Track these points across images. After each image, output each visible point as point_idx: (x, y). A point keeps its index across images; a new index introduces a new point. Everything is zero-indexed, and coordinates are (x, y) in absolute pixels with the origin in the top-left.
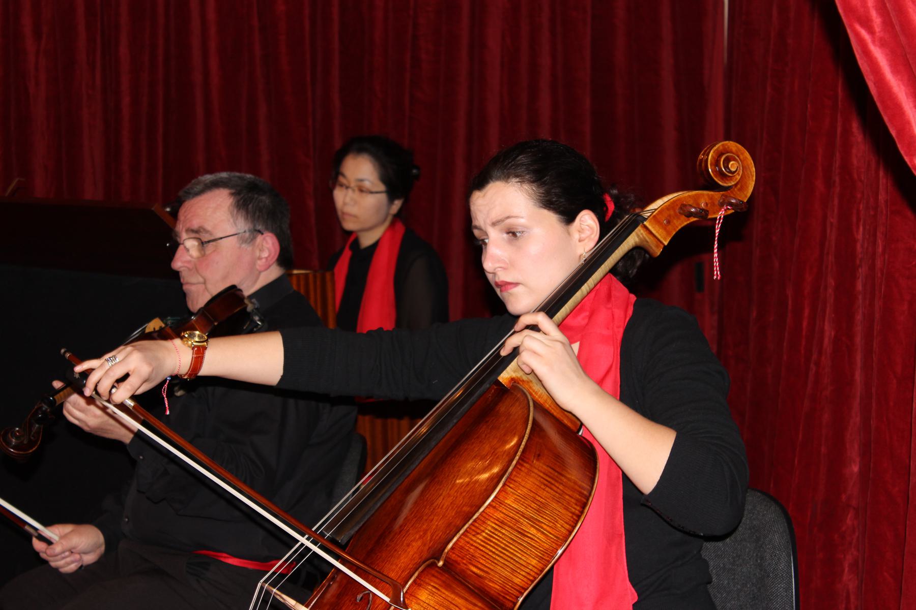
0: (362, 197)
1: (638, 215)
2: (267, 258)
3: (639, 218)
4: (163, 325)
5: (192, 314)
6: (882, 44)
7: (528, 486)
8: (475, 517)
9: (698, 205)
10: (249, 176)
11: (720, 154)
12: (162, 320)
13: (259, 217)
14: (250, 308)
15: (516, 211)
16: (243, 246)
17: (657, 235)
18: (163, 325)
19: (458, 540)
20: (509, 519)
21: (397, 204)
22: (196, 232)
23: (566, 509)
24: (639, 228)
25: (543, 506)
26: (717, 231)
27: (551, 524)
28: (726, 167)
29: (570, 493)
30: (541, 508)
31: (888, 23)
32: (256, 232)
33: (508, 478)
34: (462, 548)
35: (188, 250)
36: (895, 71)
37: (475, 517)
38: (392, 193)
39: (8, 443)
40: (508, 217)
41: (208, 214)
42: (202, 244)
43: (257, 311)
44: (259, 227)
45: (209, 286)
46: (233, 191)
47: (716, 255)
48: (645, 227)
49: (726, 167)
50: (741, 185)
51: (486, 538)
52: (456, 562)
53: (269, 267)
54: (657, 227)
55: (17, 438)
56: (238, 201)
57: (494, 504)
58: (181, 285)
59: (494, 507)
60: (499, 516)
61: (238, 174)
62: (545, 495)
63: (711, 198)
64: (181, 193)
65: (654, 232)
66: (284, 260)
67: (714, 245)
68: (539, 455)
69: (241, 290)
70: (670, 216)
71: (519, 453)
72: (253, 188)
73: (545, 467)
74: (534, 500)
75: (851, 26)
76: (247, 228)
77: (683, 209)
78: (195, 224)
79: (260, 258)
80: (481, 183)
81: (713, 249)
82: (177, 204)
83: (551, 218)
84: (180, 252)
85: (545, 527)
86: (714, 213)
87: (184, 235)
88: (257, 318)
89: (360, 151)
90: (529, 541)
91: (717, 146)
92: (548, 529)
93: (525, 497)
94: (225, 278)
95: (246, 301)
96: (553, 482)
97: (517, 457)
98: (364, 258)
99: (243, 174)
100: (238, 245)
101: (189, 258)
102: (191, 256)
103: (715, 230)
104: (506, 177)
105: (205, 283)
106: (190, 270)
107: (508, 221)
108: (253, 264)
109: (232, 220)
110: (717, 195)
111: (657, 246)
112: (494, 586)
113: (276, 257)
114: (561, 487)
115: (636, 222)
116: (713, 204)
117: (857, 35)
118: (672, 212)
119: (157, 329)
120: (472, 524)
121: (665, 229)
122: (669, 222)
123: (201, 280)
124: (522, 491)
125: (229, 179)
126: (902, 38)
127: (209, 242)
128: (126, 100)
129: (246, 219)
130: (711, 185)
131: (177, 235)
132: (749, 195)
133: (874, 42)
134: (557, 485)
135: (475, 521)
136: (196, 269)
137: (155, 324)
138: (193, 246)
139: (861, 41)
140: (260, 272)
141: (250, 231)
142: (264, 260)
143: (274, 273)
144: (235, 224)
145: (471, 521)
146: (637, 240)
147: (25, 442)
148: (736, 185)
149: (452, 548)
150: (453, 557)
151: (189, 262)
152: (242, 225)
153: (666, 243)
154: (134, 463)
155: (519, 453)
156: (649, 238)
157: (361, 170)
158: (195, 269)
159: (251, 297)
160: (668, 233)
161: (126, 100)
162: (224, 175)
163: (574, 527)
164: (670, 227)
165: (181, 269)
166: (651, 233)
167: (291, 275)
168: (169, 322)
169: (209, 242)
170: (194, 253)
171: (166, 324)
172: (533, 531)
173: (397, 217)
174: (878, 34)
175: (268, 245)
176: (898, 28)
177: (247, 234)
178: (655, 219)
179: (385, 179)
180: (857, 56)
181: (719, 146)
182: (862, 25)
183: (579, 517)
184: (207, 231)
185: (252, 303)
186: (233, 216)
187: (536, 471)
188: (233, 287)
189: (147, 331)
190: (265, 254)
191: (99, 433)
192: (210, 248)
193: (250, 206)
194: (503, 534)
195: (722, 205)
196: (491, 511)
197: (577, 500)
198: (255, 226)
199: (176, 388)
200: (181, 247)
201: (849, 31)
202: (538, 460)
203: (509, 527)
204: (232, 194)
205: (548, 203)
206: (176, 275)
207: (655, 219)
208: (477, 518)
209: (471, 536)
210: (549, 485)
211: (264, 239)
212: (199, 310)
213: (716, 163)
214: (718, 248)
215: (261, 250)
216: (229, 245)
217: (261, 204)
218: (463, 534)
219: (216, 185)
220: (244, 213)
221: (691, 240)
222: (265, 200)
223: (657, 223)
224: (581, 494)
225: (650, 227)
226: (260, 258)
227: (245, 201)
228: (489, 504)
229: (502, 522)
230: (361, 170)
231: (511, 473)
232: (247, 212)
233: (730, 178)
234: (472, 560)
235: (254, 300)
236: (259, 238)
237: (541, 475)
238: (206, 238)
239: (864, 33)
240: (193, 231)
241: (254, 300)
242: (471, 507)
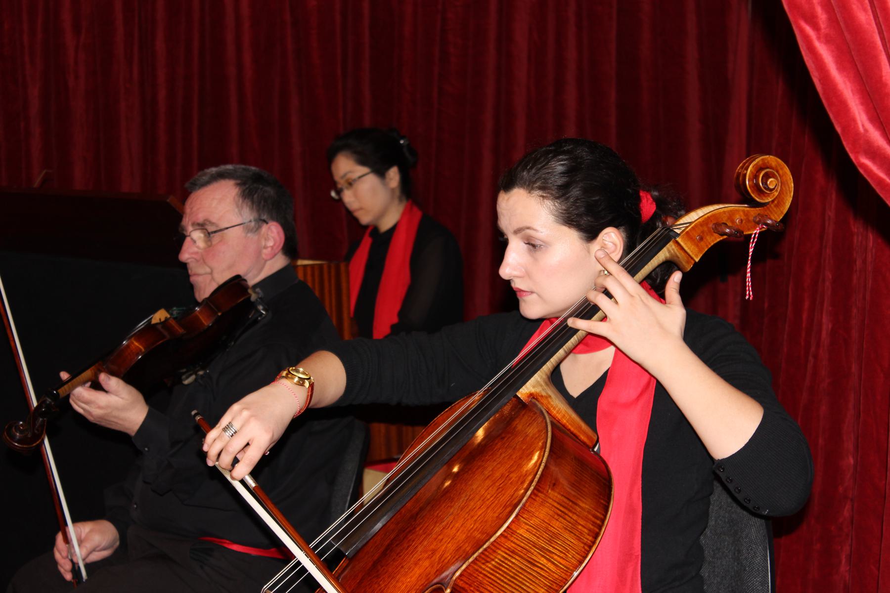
1: (669, 230)
2: (272, 247)
3: (671, 234)
4: (169, 316)
5: (197, 304)
6: (828, 40)
7: (541, 516)
8: (485, 546)
9: (733, 222)
10: (253, 168)
11: (759, 169)
12: (168, 311)
13: (264, 206)
14: (254, 297)
15: (537, 225)
16: (249, 235)
17: (688, 251)
18: (169, 316)
19: (467, 568)
20: (519, 548)
21: (394, 175)
22: (201, 226)
23: (579, 539)
24: (671, 243)
25: (553, 538)
26: (751, 250)
27: (562, 555)
28: (765, 183)
29: (582, 522)
30: (553, 538)
31: (833, 20)
32: (260, 221)
33: (521, 508)
34: (471, 575)
35: (195, 242)
36: (841, 68)
37: (485, 546)
39: (13, 437)
40: (528, 228)
41: (214, 205)
42: (209, 235)
43: (262, 300)
44: (265, 217)
45: (216, 275)
46: (239, 182)
47: (749, 275)
48: (677, 242)
49: (765, 183)
50: (778, 202)
51: (495, 567)
52: (463, 589)
53: (275, 255)
54: (689, 244)
55: (21, 432)
56: (244, 191)
57: (506, 534)
58: (188, 276)
59: (506, 537)
60: (509, 544)
61: (243, 166)
62: (557, 525)
63: (746, 214)
64: (187, 185)
65: (686, 248)
66: (290, 249)
67: (747, 264)
68: (554, 485)
69: (245, 280)
70: (703, 232)
71: (534, 484)
72: (257, 179)
73: (559, 496)
74: (547, 530)
75: (796, 22)
76: (252, 218)
78: (201, 217)
79: (265, 247)
81: (746, 269)
82: (185, 195)
84: (187, 246)
85: (556, 557)
86: (749, 230)
87: (190, 228)
88: (260, 307)
90: (539, 570)
91: (757, 160)
92: (559, 559)
93: (537, 528)
94: (230, 267)
95: (250, 291)
96: (567, 512)
97: (532, 488)
98: (382, 240)
99: (248, 167)
100: (243, 235)
101: (196, 249)
102: (198, 247)
103: (748, 249)
105: (211, 273)
106: (197, 261)
107: (528, 231)
108: (259, 253)
109: (236, 210)
110: (754, 212)
111: (688, 262)
113: (282, 245)
114: (575, 517)
115: (669, 236)
116: (748, 221)
117: (802, 31)
118: (706, 229)
119: (163, 320)
120: (482, 553)
121: (697, 246)
122: (701, 239)
123: (208, 270)
124: (534, 521)
125: (235, 170)
126: (848, 36)
127: (215, 232)
129: (252, 209)
130: (745, 198)
131: (184, 229)
132: (785, 211)
133: (819, 38)
134: (570, 514)
135: (485, 550)
136: (203, 260)
138: (200, 238)
139: (807, 38)
140: (266, 261)
141: (255, 220)
142: (269, 249)
143: (279, 262)
144: (241, 214)
145: (481, 551)
146: (668, 255)
147: (29, 436)
148: (773, 201)
149: (461, 575)
150: (461, 584)
151: (197, 253)
152: (247, 215)
153: (697, 260)
154: (138, 453)
155: (534, 484)
156: (680, 254)
158: (203, 260)
159: (255, 286)
160: (700, 250)
162: (229, 167)
163: (585, 558)
164: (702, 243)
165: (189, 261)
166: (682, 249)
167: (296, 267)
168: (175, 313)
169: (215, 232)
170: (201, 244)
171: (171, 314)
172: (543, 561)
174: (823, 31)
175: (273, 234)
176: (842, 24)
177: (253, 224)
178: (688, 235)
180: (803, 53)
181: (758, 160)
182: (806, 21)
183: (590, 547)
184: (212, 224)
185: (255, 292)
186: (238, 206)
187: (550, 501)
188: (238, 277)
189: (154, 322)
190: (270, 243)
191: (104, 424)
192: (216, 238)
193: (256, 196)
194: (513, 563)
195: (758, 223)
196: (503, 539)
197: (590, 530)
198: (260, 215)
199: (184, 377)
200: (188, 239)
201: (794, 28)
202: (552, 490)
203: (520, 556)
204: (238, 184)
205: (569, 220)
206: (184, 266)
207: (688, 235)
208: (488, 547)
209: (479, 564)
210: (562, 515)
211: (269, 228)
212: (203, 301)
213: (755, 176)
214: (751, 267)
215: (267, 239)
216: (235, 235)
217: (266, 195)
218: (472, 562)
219: (221, 176)
220: (249, 203)
222: (270, 191)
224: (594, 524)
225: (682, 244)
226: (265, 247)
227: (250, 191)
228: (501, 534)
229: (513, 552)
231: (524, 505)
232: (253, 203)
233: (768, 195)
235: (258, 290)
236: (265, 228)
237: (555, 504)
238: (211, 229)
239: (808, 29)
240: (199, 224)
241: (258, 290)
242: (482, 533)
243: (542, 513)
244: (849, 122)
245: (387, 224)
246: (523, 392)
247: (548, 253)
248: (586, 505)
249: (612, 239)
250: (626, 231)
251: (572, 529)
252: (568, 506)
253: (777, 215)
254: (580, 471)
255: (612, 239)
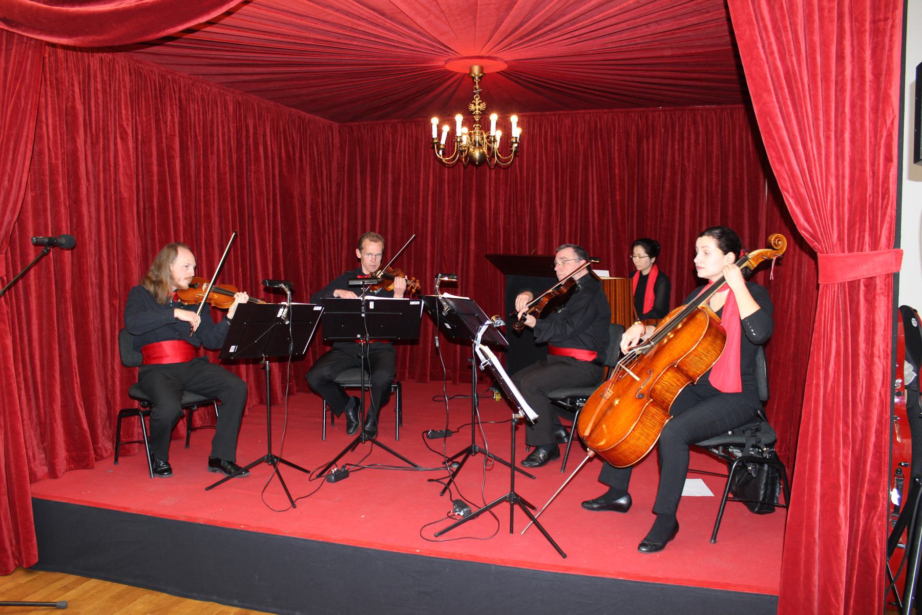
0: (642, 259)
6: (792, 197)
21: (653, 260)
25: (708, 352)
30: (708, 352)
31: (794, 191)
36: (796, 205)
38: (651, 256)
50: (782, 249)
62: (710, 348)
77: (761, 255)
80: (701, 235)
83: (720, 252)
89: (638, 244)
98: (643, 279)
104: (709, 235)
112: (691, 374)
128: (567, 227)
137: (215, 597)
157: (639, 251)
161: (567, 227)
173: (654, 264)
179: (647, 252)
205: (720, 247)
207: (753, 259)
221: (765, 265)
223: (754, 256)
230: (639, 251)
234: (685, 365)
243: (705, 344)
244: (798, 221)
245: (645, 273)
246: (700, 306)
247: (710, 257)
248: (719, 342)
249: (731, 256)
250: (644, 246)
251: (714, 349)
252: (714, 342)
253: (780, 254)
254: (717, 332)
255: (731, 256)
